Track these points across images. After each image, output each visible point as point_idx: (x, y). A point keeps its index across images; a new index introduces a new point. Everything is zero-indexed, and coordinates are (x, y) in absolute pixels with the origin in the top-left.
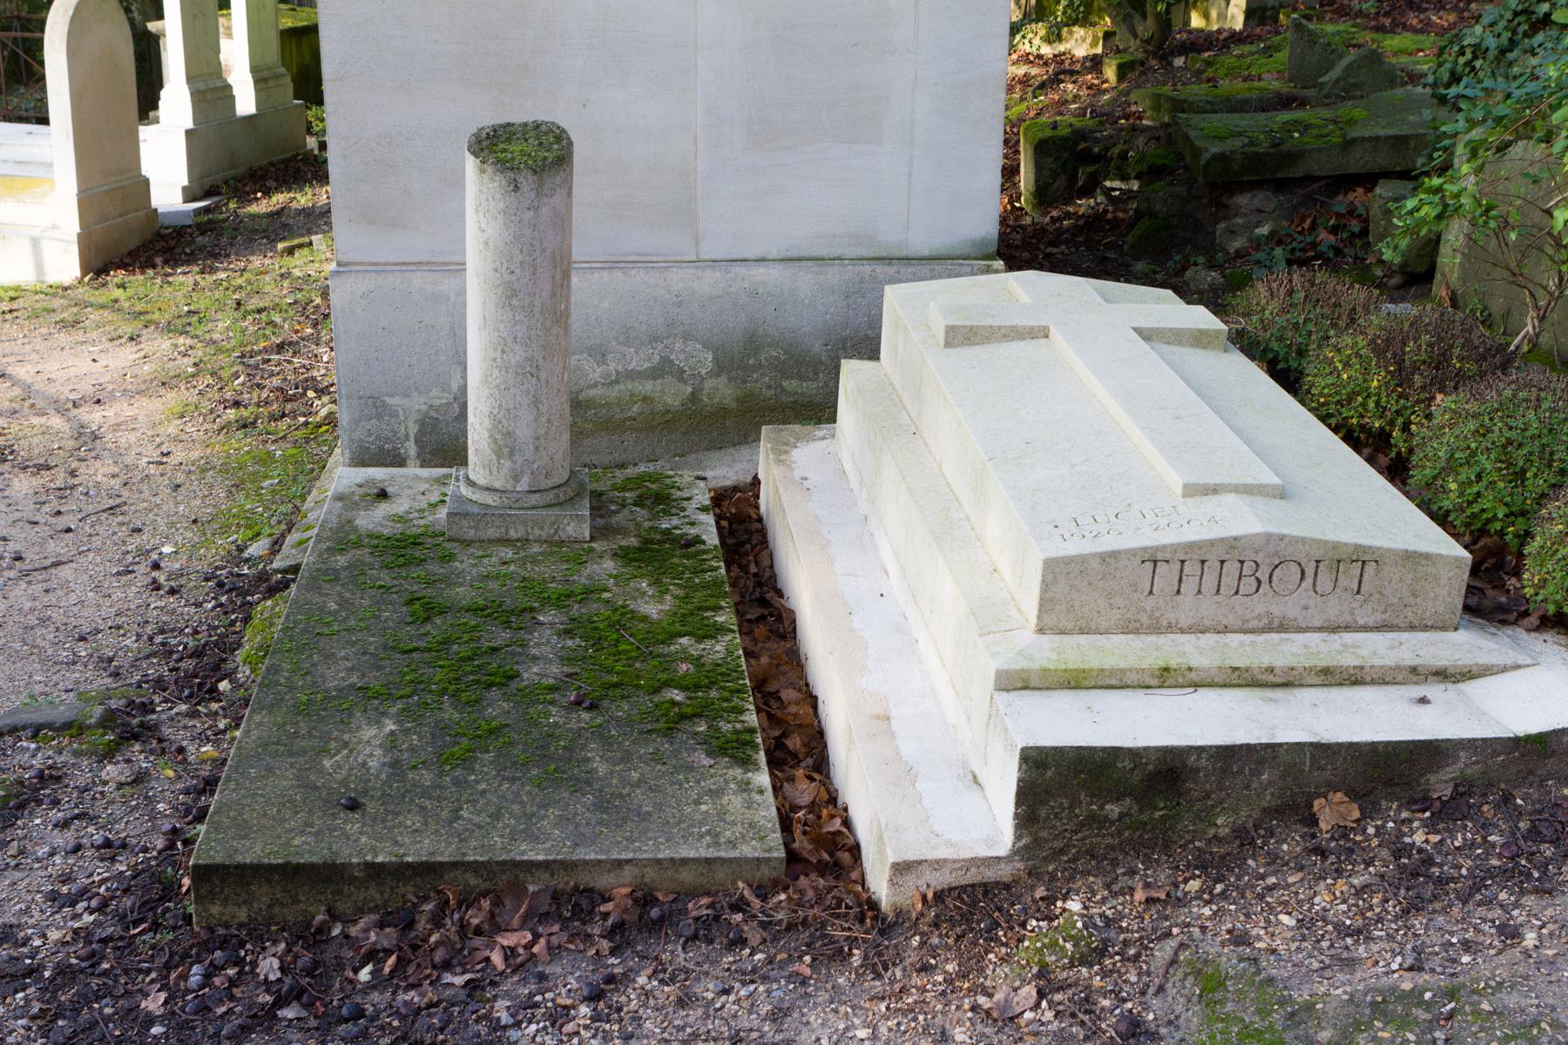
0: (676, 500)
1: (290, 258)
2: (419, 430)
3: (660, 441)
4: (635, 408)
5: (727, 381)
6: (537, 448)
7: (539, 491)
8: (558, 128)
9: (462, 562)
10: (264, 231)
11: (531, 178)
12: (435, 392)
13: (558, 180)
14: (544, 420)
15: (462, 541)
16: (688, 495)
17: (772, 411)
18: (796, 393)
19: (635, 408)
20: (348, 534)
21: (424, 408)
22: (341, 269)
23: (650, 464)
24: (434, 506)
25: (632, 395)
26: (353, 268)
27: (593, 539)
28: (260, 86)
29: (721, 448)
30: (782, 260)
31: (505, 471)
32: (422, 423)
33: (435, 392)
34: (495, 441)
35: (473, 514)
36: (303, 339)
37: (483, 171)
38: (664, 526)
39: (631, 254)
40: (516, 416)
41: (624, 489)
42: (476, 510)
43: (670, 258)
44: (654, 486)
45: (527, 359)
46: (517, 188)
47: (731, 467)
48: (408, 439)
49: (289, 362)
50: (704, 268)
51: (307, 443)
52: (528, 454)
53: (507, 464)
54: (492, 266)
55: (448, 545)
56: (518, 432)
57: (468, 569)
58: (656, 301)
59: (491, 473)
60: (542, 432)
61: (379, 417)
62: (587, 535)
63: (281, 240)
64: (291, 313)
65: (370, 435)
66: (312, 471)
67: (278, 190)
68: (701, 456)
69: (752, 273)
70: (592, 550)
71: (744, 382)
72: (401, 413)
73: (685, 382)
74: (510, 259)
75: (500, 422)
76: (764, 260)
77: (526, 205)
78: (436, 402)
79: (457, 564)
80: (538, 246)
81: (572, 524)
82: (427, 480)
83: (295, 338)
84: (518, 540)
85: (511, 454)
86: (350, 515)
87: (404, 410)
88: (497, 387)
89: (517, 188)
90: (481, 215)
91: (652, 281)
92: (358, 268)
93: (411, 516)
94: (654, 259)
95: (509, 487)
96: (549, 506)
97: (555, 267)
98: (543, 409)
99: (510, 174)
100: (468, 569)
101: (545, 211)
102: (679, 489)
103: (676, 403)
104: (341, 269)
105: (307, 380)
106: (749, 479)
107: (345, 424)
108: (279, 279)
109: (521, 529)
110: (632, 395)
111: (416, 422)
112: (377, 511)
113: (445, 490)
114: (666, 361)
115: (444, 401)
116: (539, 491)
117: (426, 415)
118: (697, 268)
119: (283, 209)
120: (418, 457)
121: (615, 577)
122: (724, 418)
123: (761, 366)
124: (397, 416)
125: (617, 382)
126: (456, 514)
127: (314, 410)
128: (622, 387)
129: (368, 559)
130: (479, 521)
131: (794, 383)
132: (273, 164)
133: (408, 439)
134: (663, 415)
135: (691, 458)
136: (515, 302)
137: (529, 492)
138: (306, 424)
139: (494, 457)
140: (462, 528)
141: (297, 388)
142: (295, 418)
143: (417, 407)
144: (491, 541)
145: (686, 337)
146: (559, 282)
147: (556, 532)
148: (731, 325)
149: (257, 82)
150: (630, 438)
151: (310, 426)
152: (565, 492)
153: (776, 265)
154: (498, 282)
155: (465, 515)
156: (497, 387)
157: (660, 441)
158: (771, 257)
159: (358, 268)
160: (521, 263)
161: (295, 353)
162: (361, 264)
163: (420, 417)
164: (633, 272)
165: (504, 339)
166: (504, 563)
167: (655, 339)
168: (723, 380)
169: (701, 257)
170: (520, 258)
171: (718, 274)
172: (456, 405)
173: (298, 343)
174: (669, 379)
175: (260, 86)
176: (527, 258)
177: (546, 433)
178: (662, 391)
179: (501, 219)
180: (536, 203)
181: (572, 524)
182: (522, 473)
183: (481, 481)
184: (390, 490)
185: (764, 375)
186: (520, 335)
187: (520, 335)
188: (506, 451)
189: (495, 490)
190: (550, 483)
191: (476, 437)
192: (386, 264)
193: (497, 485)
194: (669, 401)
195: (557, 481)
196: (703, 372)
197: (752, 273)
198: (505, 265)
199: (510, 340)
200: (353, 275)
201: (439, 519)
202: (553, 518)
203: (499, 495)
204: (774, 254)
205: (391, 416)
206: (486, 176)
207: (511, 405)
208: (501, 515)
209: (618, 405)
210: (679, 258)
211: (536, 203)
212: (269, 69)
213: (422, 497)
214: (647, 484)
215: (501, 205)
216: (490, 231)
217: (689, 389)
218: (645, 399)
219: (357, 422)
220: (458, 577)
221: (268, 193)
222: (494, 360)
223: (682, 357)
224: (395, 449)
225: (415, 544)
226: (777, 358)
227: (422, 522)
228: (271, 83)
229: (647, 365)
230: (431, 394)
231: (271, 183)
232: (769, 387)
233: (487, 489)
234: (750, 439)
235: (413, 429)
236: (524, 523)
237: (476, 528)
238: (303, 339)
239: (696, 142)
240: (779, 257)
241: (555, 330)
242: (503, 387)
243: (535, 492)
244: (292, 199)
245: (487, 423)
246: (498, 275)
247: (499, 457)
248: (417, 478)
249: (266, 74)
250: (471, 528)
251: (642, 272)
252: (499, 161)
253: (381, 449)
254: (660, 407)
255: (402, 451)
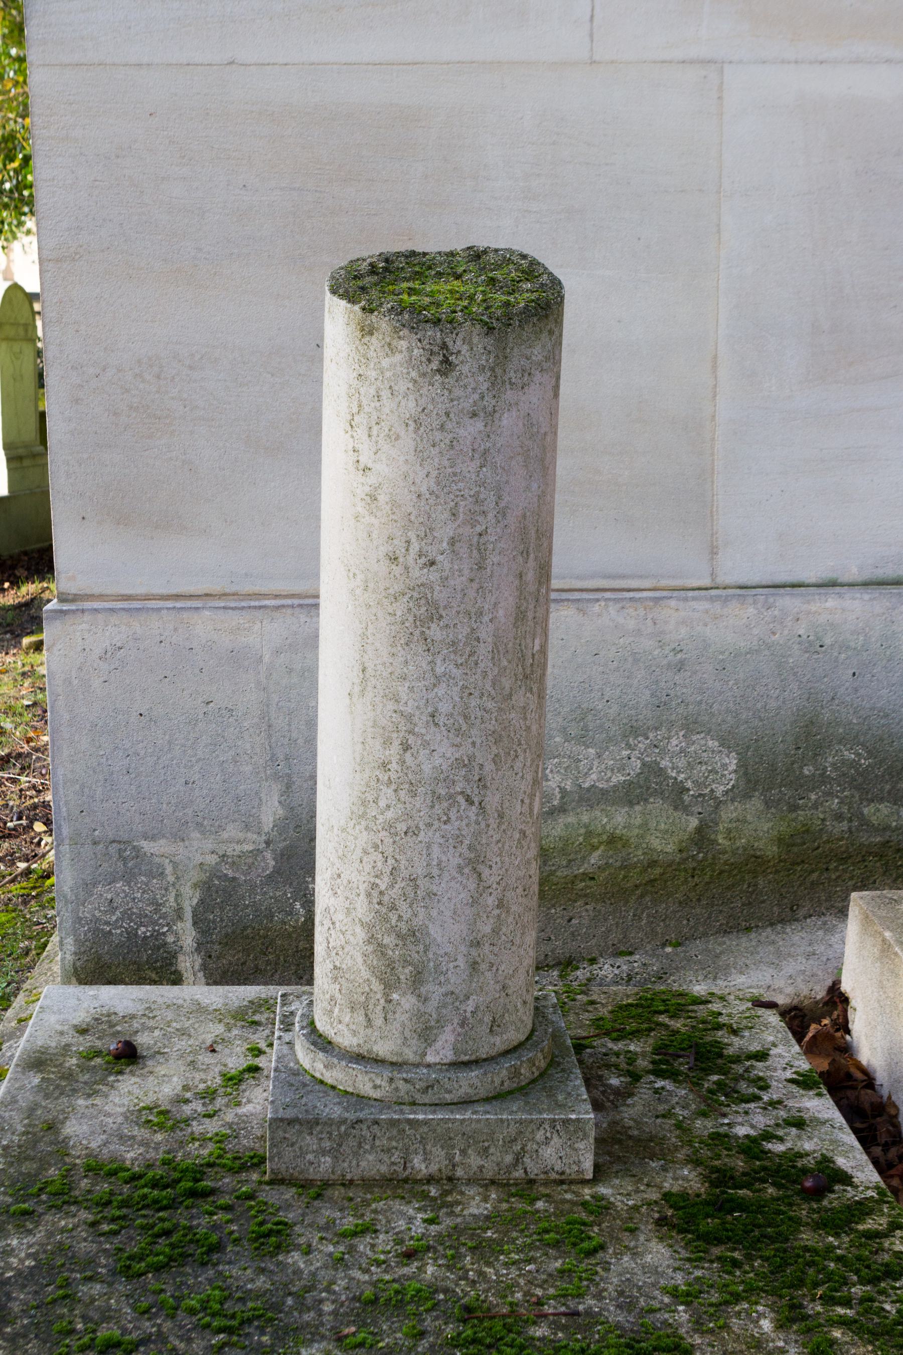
0: (737, 1060)
1: (36, 655)
2: (202, 901)
3: (637, 917)
4: (595, 858)
5: (760, 806)
6: (474, 966)
7: (477, 1062)
8: (524, 257)
9: (308, 1251)
10: (8, 625)
11: (479, 341)
12: (232, 831)
13: (537, 353)
14: (491, 901)
15: (304, 1185)
16: (755, 1047)
17: (843, 860)
18: (887, 828)
19: (595, 858)
20: (44, 1165)
21: (212, 859)
22: (65, 607)
23: (620, 961)
24: (234, 1081)
25: (589, 834)
26: (88, 605)
27: (600, 1173)
28: (14, 464)
29: (748, 929)
30: (866, 584)
31: (401, 1017)
32: (206, 886)
33: (232, 831)
34: (381, 950)
35: (330, 1122)
36: (37, 750)
37: (367, 331)
38: (741, 1131)
39: (592, 577)
40: (431, 895)
41: (622, 1035)
42: (334, 1110)
43: (664, 583)
44: (677, 1024)
45: (459, 763)
46: (447, 366)
47: (779, 968)
48: (180, 918)
49: (14, 781)
50: (726, 600)
51: (25, 903)
52: (456, 979)
53: (407, 1002)
54: (383, 549)
55: (271, 1196)
56: (434, 931)
57: (325, 1275)
58: (636, 661)
59: (369, 1022)
60: (487, 929)
61: (129, 877)
62: (588, 1165)
63: (28, 634)
64: (27, 717)
65: (113, 910)
66: (27, 952)
67: (29, 579)
68: (714, 944)
69: (813, 607)
70: (602, 1208)
71: (794, 808)
72: (169, 869)
73: (686, 810)
74: (428, 533)
75: (393, 908)
76: (833, 584)
77: (467, 405)
78: (234, 849)
79: (295, 1258)
80: (490, 504)
81: (556, 1141)
82: (218, 1015)
83: (26, 748)
84: (430, 1180)
85: (418, 979)
86: (52, 1108)
87: (175, 865)
88: (389, 827)
89: (447, 366)
90: (361, 433)
91: (631, 624)
92: (96, 605)
93: (187, 1109)
94: (634, 584)
95: (410, 1055)
96: (498, 1097)
97: (526, 553)
98: (491, 877)
99: (431, 332)
100: (325, 1275)
101: (508, 421)
102: (735, 1032)
103: (670, 848)
104: (65, 607)
105: (35, 807)
106: (820, 993)
107: (66, 889)
108: (19, 678)
109: (439, 1153)
110: (589, 834)
111: (195, 886)
112: (114, 1097)
113: (259, 1039)
114: (652, 770)
115: (250, 847)
116: (477, 1062)
117: (215, 873)
118: (712, 599)
119: (32, 600)
120: (198, 950)
121: (686, 1297)
122: (755, 874)
123: (824, 779)
124: (162, 874)
125: (562, 809)
126: (291, 1122)
127: (40, 851)
128: (571, 819)
129: (85, 1247)
130: (344, 1137)
131: (885, 809)
132: (25, 553)
133: (180, 918)
134: (644, 870)
135: (695, 948)
136: (435, 631)
137: (457, 1065)
138: (28, 872)
139: (377, 986)
140: (303, 1153)
141: (20, 818)
142: (13, 863)
143: (198, 859)
144: (368, 1184)
145: (691, 726)
146: (532, 588)
147: (518, 1159)
148: (773, 704)
149: (9, 460)
150: (583, 913)
151: (34, 876)
152: (531, 1062)
153: (857, 593)
154: (397, 587)
155: (312, 1124)
156: (389, 827)
157: (637, 917)
158: (846, 578)
159: (96, 605)
160: (452, 542)
161: (23, 769)
162: (101, 597)
163: (204, 877)
164: (596, 608)
165: (409, 718)
166: (410, 1255)
167: (634, 731)
168: (756, 803)
169: (721, 579)
170: (449, 531)
171: (751, 610)
172: (268, 855)
173: (29, 755)
174: (656, 804)
175: (14, 464)
176: (467, 530)
177: (496, 931)
178: (644, 825)
179: (408, 440)
180: (489, 402)
181: (556, 1141)
182: (441, 1023)
183: (346, 1039)
184: (143, 1040)
185: (829, 794)
186: (444, 708)
187: (444, 708)
188: (405, 973)
189: (379, 1061)
190: (500, 1042)
191: (336, 940)
192: (148, 598)
193: (383, 1049)
194: (656, 843)
195: (514, 1036)
196: (720, 790)
197: (813, 607)
198: (415, 547)
199: (420, 720)
200: (87, 617)
201: (244, 1120)
202: (513, 1130)
203: (387, 1074)
204: (853, 573)
205: (151, 875)
206: (375, 341)
207: (419, 870)
208: (393, 1123)
209: (563, 851)
210: (678, 583)
211: (489, 402)
212: (26, 447)
213: (206, 1058)
214: (663, 1019)
215: (410, 406)
216: (381, 468)
217: (694, 822)
218: (613, 840)
219: (88, 886)
220: (302, 1307)
221: (16, 583)
222: (385, 766)
223: (681, 763)
224: (157, 935)
225: (193, 1194)
226: (854, 764)
227: (212, 1127)
228: (26, 462)
229: (618, 778)
230: (225, 835)
231: (21, 572)
232: (839, 817)
233: (359, 1058)
234: (801, 913)
235: (190, 899)
236: (446, 1141)
237: (335, 1153)
238: (37, 750)
239: (715, 367)
240: (860, 579)
241: (520, 698)
242: (402, 827)
243: (467, 1064)
244: (44, 590)
245: (362, 908)
246: (397, 570)
247: (389, 986)
248: (199, 1009)
249: (21, 451)
250: (324, 1153)
251: (613, 609)
252: (398, 310)
253: (132, 935)
254: (638, 856)
255: (170, 939)
